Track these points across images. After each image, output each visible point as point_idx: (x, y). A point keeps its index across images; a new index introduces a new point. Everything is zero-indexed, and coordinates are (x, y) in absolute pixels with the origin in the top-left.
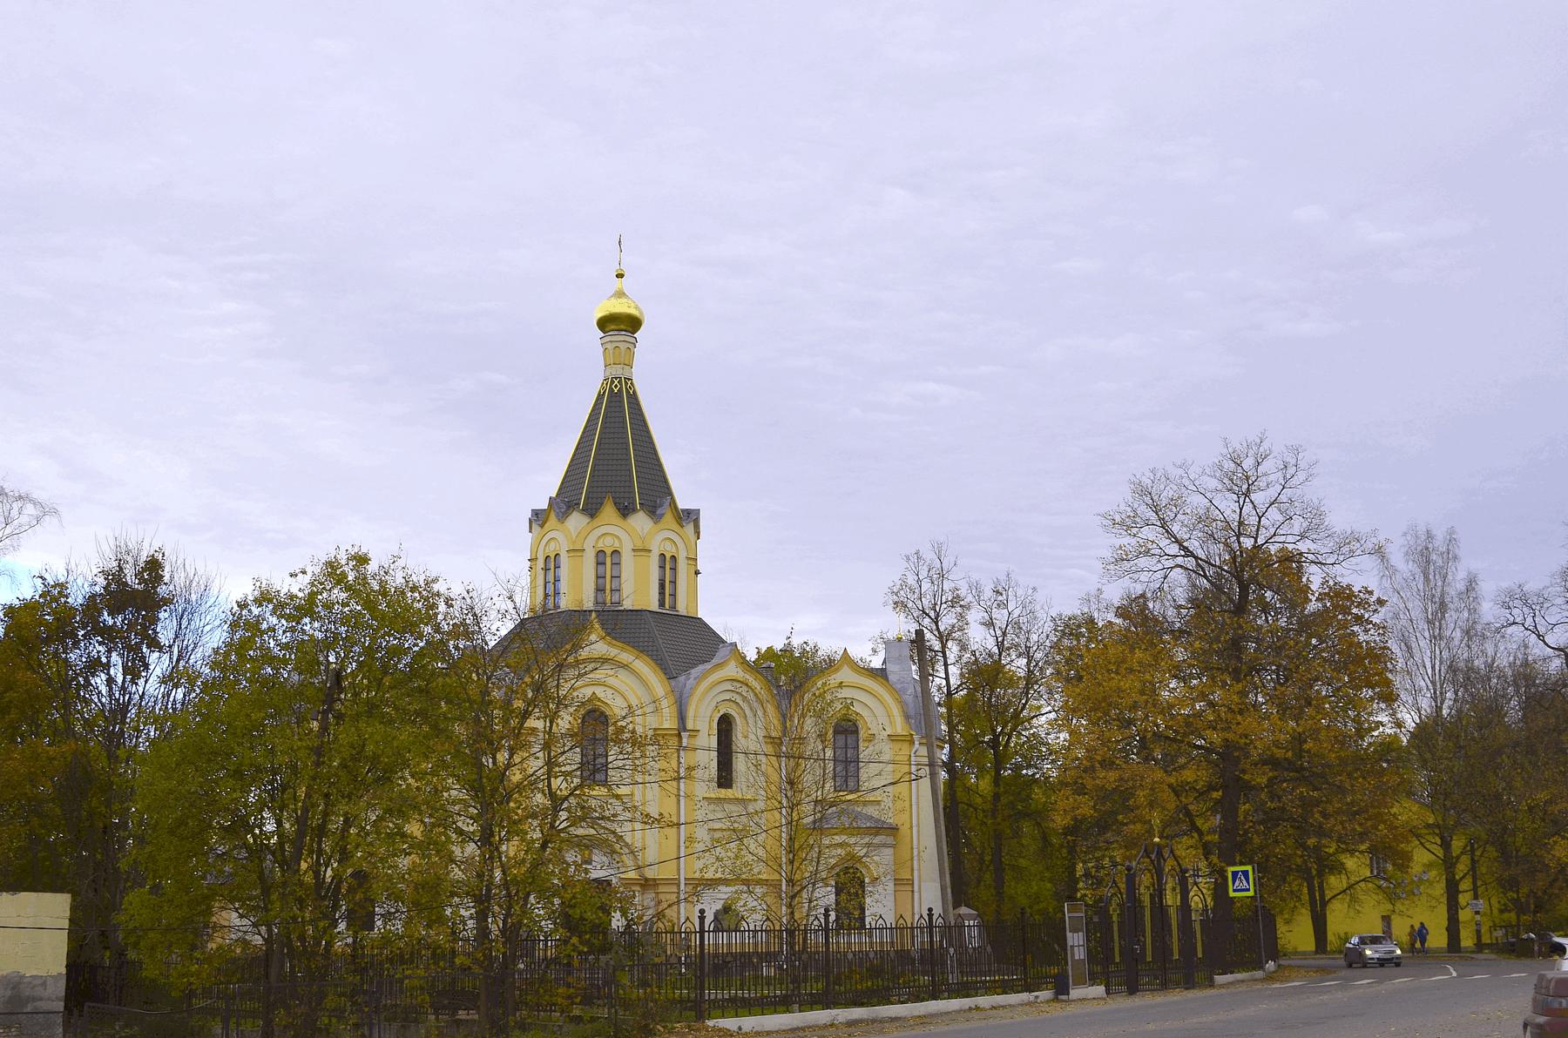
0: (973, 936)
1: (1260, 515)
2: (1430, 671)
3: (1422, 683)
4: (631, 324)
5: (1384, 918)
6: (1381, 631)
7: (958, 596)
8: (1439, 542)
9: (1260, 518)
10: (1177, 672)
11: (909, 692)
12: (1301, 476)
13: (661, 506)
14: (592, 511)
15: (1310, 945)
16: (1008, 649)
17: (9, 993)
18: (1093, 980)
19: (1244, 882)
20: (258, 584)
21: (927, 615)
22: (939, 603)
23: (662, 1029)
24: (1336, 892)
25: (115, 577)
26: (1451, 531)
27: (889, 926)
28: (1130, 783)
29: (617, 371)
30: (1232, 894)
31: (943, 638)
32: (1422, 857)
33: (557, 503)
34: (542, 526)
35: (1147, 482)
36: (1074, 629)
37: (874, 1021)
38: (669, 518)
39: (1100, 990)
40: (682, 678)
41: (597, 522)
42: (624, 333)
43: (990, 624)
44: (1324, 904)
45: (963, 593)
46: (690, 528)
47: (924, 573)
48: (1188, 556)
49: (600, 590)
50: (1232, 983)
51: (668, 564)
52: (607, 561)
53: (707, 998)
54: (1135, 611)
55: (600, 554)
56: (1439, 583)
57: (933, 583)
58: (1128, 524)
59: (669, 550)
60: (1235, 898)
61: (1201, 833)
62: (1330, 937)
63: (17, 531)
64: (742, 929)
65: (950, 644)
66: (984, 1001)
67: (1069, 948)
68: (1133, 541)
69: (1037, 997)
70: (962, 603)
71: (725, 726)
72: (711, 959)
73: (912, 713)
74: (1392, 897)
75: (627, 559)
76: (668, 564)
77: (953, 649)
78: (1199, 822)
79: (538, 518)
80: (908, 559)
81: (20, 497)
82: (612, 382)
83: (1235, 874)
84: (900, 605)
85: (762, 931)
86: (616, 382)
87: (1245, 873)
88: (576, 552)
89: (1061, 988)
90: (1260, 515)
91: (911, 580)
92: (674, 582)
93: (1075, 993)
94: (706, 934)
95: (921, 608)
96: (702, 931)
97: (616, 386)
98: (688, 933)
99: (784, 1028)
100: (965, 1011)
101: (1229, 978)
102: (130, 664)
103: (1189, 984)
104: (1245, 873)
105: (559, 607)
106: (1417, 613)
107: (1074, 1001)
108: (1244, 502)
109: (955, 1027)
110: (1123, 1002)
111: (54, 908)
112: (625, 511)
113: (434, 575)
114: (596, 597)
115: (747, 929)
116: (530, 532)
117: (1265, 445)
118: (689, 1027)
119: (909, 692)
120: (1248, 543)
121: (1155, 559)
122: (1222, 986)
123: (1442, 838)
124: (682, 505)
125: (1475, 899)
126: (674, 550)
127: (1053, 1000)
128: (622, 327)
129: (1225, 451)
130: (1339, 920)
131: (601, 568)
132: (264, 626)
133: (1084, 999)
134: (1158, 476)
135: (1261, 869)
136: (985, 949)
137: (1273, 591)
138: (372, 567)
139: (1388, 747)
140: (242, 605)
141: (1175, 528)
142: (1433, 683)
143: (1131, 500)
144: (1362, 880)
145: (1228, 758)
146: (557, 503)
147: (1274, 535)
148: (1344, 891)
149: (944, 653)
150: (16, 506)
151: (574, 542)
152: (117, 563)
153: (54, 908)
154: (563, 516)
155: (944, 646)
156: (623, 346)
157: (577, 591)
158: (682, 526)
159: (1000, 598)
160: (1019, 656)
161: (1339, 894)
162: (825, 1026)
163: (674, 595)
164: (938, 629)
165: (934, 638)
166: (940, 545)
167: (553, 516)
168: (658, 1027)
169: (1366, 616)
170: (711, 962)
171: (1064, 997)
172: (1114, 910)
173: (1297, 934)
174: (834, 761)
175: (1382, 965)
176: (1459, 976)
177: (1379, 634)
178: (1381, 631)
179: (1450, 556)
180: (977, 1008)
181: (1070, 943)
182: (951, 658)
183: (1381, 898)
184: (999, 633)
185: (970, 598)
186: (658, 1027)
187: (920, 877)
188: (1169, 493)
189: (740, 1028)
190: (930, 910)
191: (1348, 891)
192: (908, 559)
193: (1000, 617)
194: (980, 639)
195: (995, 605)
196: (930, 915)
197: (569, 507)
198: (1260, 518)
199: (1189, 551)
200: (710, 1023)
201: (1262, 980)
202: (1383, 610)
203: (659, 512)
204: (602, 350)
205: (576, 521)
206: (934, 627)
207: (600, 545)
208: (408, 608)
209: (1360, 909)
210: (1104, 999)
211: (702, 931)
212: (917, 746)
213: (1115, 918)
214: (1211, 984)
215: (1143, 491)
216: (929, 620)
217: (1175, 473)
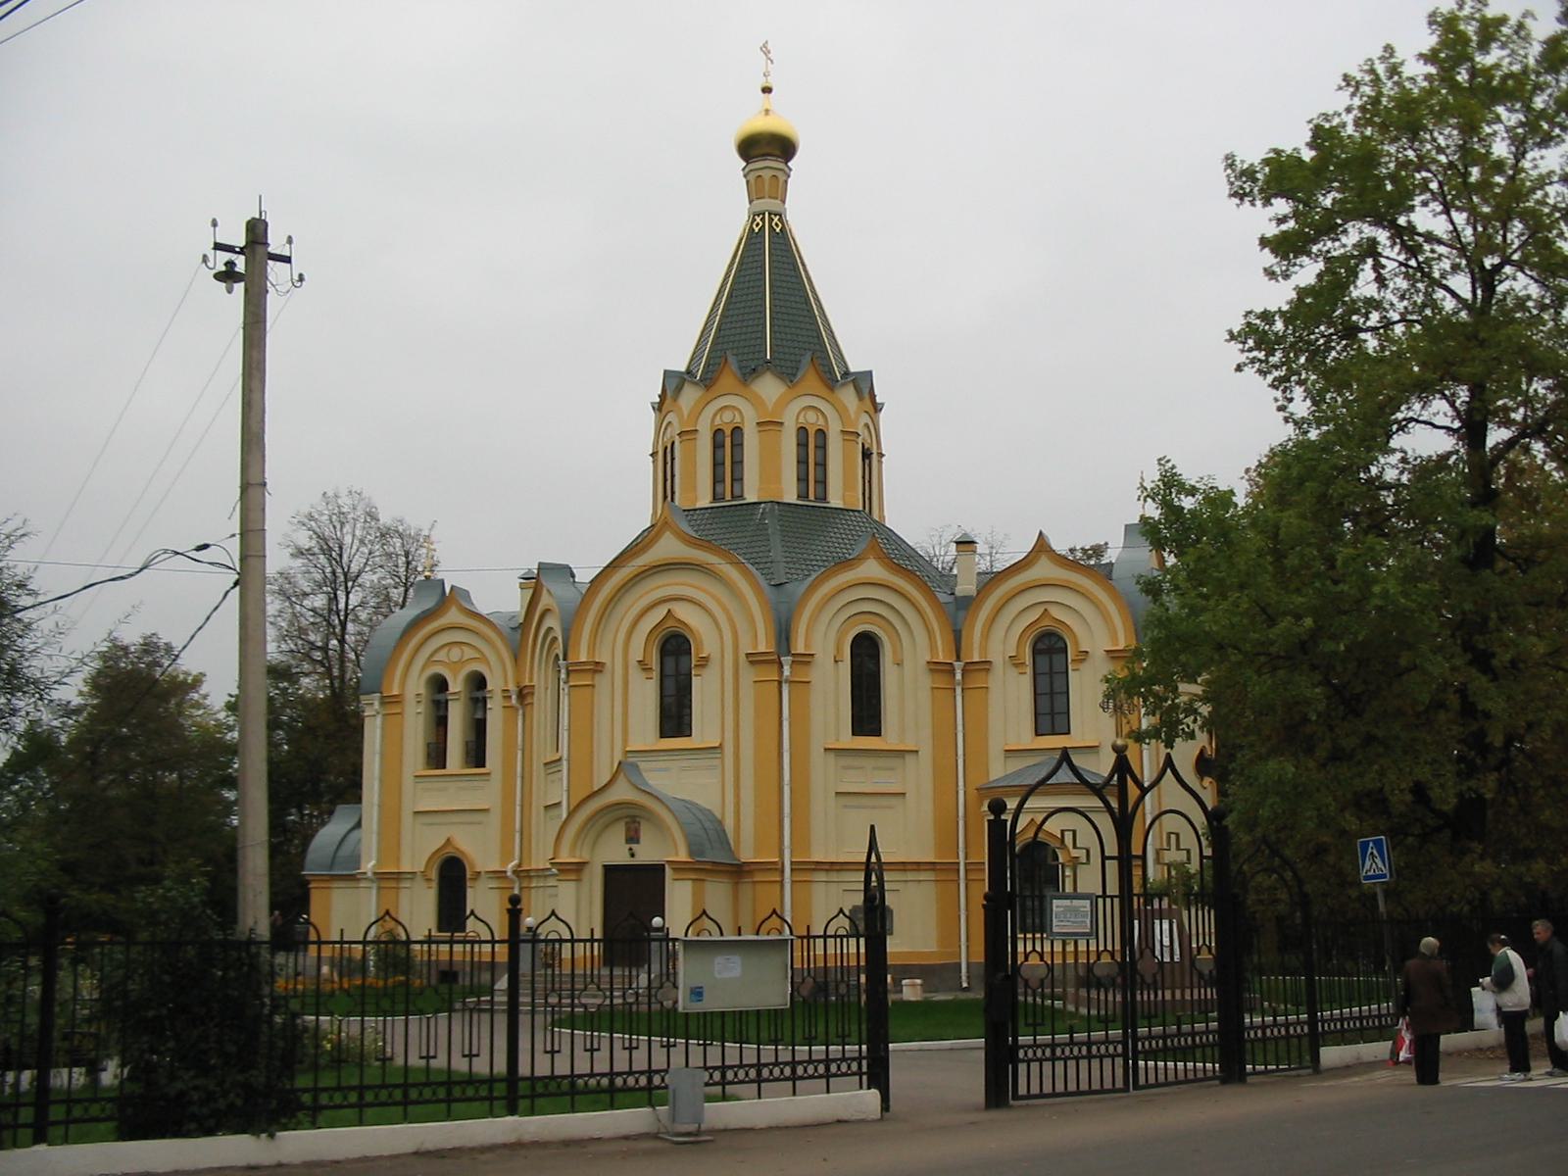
41: (718, 388)
51: (812, 447)
59: (812, 420)
71: (865, 652)
76: (812, 447)
97: (758, 225)
98: (842, 937)
102: (1292, 355)
112: (750, 373)
116: (659, 407)
126: (821, 421)
174: (572, 1075)
207: (718, 421)
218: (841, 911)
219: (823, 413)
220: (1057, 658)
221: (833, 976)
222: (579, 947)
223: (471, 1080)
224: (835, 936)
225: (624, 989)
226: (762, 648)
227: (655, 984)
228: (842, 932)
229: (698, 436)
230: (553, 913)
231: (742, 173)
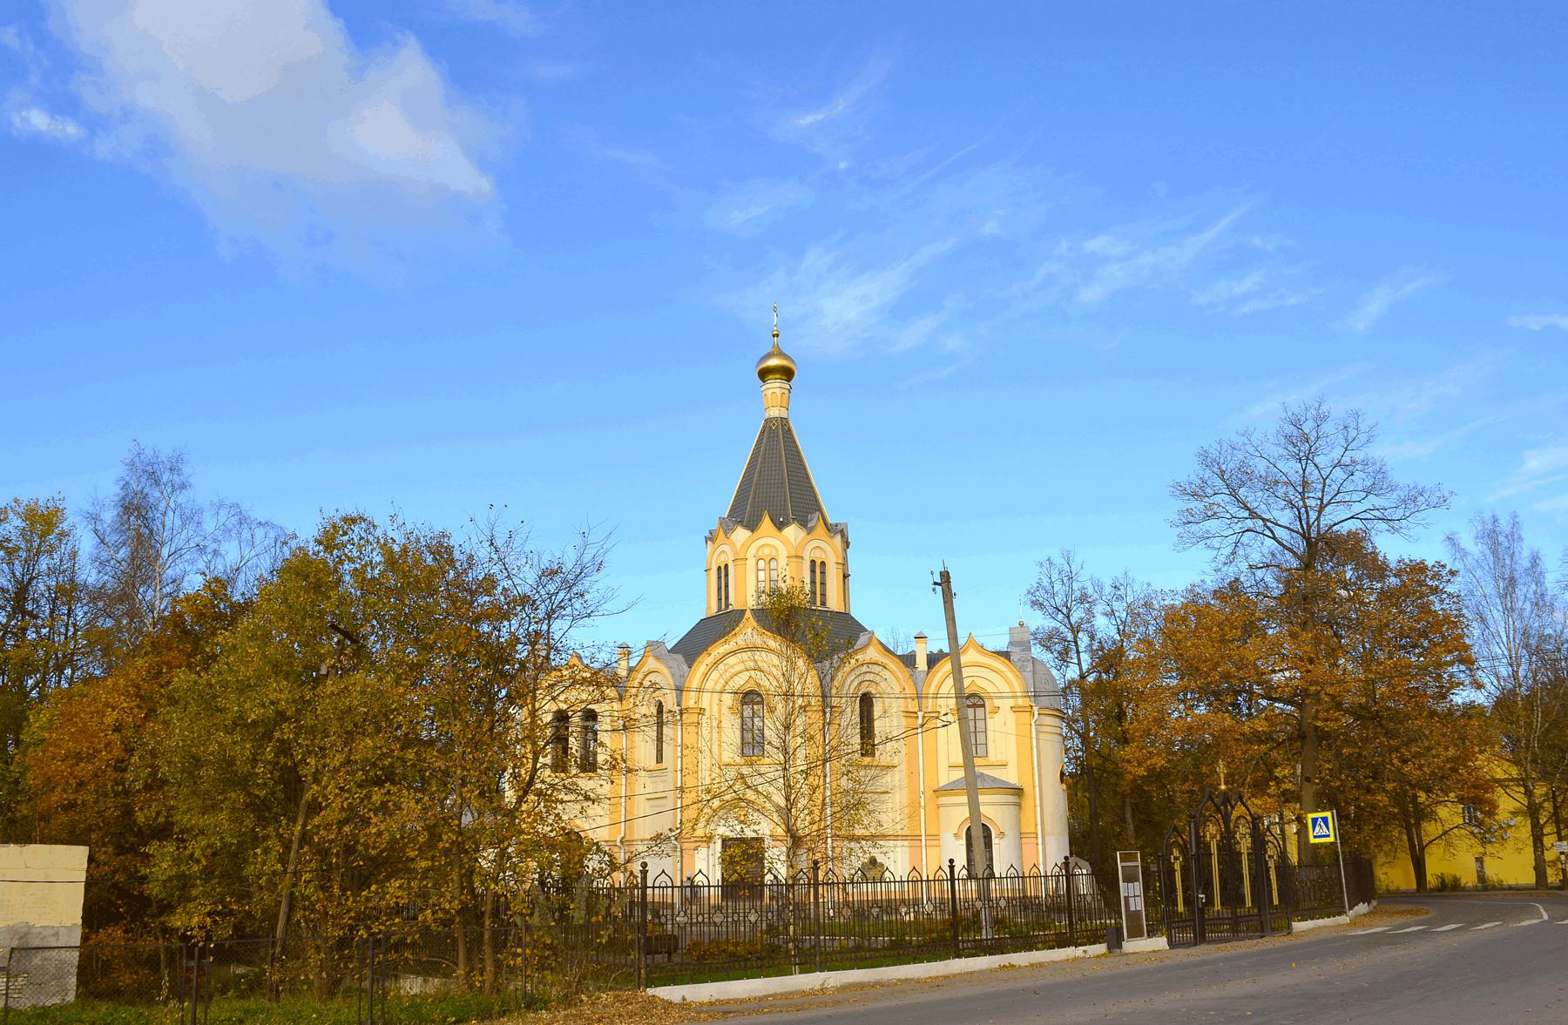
2: (1505, 639)
3: (1500, 652)
5: (1477, 859)
6: (1455, 600)
8: (1504, 525)
9: (1324, 480)
12: (1363, 438)
14: (752, 526)
19: (1324, 828)
22: (1070, 601)
24: (1432, 838)
26: (1514, 516)
27: (925, 878)
30: (1313, 841)
31: (1075, 630)
32: (1507, 803)
35: (1213, 453)
38: (821, 529)
44: (1422, 849)
45: (1090, 591)
47: (1055, 576)
56: (1508, 562)
59: (819, 557)
62: (1429, 877)
64: (888, 880)
65: (1080, 635)
68: (1201, 506)
69: (1085, 952)
72: (962, 904)
74: (1484, 842)
77: (1084, 640)
83: (1315, 821)
84: (1036, 604)
91: (1045, 583)
94: (956, 881)
96: (952, 880)
98: (663, 887)
104: (1325, 820)
106: (1490, 589)
108: (1307, 464)
115: (892, 880)
117: (1324, 408)
123: (1526, 787)
125: (1559, 841)
129: (1283, 416)
130: (1436, 866)
135: (1341, 817)
136: (935, 907)
137: (1543, 852)
139: (1470, 710)
142: (1509, 650)
144: (1456, 827)
148: (1440, 837)
149: (1076, 642)
155: (1075, 637)
161: (1435, 840)
166: (1069, 552)
169: (1441, 587)
173: (1394, 874)
176: (1552, 918)
177: (1453, 602)
178: (1455, 600)
179: (1514, 536)
182: (1082, 646)
183: (1473, 842)
187: (1043, 830)
189: (684, 999)
190: (951, 861)
191: (1443, 837)
192: (1041, 565)
193: (1120, 607)
194: (1105, 628)
196: (952, 868)
198: (1324, 480)
202: (1459, 579)
207: (760, 554)
209: (1455, 853)
211: (952, 880)
216: (1062, 615)
218: (1056, 864)
219: (824, 550)
220: (980, 711)
221: (994, 895)
222: (657, 890)
224: (659, 887)
225: (733, 914)
227: (974, 900)
228: (965, 877)
230: (663, 871)
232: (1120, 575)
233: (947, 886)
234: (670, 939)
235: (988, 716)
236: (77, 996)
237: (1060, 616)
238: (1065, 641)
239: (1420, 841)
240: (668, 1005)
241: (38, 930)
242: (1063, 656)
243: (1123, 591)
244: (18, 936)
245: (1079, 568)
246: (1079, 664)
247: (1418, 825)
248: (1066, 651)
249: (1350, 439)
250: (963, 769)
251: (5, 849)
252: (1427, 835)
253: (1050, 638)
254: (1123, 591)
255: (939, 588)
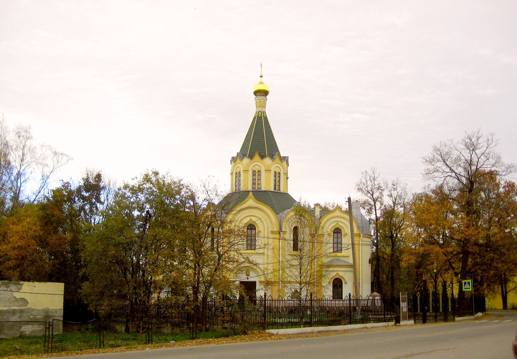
0: (379, 303)
1: (479, 158)
4: (265, 93)
7: (380, 186)
10: (454, 213)
11: (359, 219)
12: (494, 144)
13: (275, 155)
14: (251, 157)
15: (501, 306)
16: (397, 204)
17: (45, 314)
18: (410, 318)
20: (124, 182)
21: (369, 193)
22: (373, 189)
23: (250, 332)
25: (87, 180)
27: (363, 299)
28: (428, 252)
29: (260, 109)
31: (375, 201)
33: (240, 155)
34: (235, 162)
35: (438, 146)
36: (419, 198)
37: (328, 331)
38: (277, 160)
39: (412, 322)
40: (281, 214)
41: (253, 160)
42: (262, 96)
43: (391, 196)
44: (506, 293)
45: (382, 185)
46: (285, 163)
47: (368, 178)
48: (452, 172)
49: (254, 184)
50: (461, 320)
51: (277, 175)
52: (256, 174)
53: (266, 322)
54: (439, 191)
55: (254, 172)
57: (371, 181)
58: (431, 161)
59: (278, 170)
60: (466, 291)
61: (454, 269)
63: (61, 165)
65: (377, 203)
66: (369, 325)
67: (401, 307)
68: (433, 167)
69: (388, 324)
70: (381, 189)
73: (360, 226)
75: (263, 173)
76: (277, 175)
77: (378, 205)
78: (453, 265)
79: (234, 160)
80: (363, 173)
81: (62, 154)
82: (259, 113)
83: (465, 283)
84: (360, 189)
85: (287, 300)
86: (260, 113)
87: (469, 283)
88: (246, 171)
89: (398, 321)
90: (479, 158)
91: (364, 181)
92: (279, 181)
93: (402, 323)
95: (367, 190)
96: (350, 300)
97: (260, 114)
99: (294, 333)
100: (361, 328)
101: (461, 318)
103: (446, 320)
105: (240, 190)
107: (402, 325)
109: (355, 334)
110: (421, 326)
111: (59, 288)
112: (262, 157)
113: (181, 179)
114: (253, 186)
116: (231, 164)
118: (259, 332)
119: (359, 219)
120: (474, 168)
121: (440, 173)
122: (458, 321)
124: (282, 154)
127: (394, 325)
128: (262, 94)
131: (254, 176)
132: (126, 196)
133: (406, 325)
134: (442, 144)
135: (475, 281)
138: (160, 176)
140: (119, 189)
141: (448, 163)
143: (433, 152)
145: (464, 243)
146: (240, 155)
147: (483, 165)
148: (514, 288)
150: (60, 157)
151: (245, 168)
152: (87, 176)
153: (59, 288)
154: (242, 159)
155: (375, 203)
156: (262, 101)
157: (247, 184)
158: (282, 162)
159: (394, 187)
160: (401, 207)
161: (512, 290)
162: (310, 333)
163: (279, 186)
164: (373, 197)
165: (372, 201)
167: (238, 159)
168: (249, 332)
170: (268, 311)
171: (398, 324)
172: (418, 295)
175: (319, 335)
180: (366, 328)
181: (401, 306)
182: (377, 208)
184: (394, 199)
185: (384, 187)
186: (249, 332)
187: (362, 282)
188: (446, 150)
189: (278, 333)
190: (350, 294)
192: (363, 173)
193: (394, 194)
194: (388, 201)
195: (393, 189)
196: (350, 296)
197: (243, 156)
199: (453, 170)
200: (267, 331)
201: (472, 319)
203: (274, 157)
204: (255, 102)
205: (246, 160)
206: (372, 197)
207: (254, 169)
208: (172, 190)
210: (413, 325)
211: (350, 300)
212: (361, 238)
213: (418, 298)
214: (454, 320)
215: (436, 149)
216: (370, 194)
217: (448, 143)
220: (339, 235)
223: (280, 323)
224: (269, 300)
226: (275, 230)
228: (270, 299)
229: (249, 172)
231: (254, 99)
232: (395, 179)
233: (348, 302)
234: (467, 299)
235: (342, 237)
236: (63, 331)
237: (369, 195)
238: (371, 205)
239: (506, 290)
240: (273, 334)
241: (51, 310)
242: (369, 212)
243: (396, 186)
244: (45, 312)
245: (378, 175)
246: (376, 214)
247: (506, 284)
248: (371, 209)
249: (489, 144)
250: (252, 230)
251: (40, 284)
252: (509, 287)
253: (364, 203)
254: (396, 186)
255: (347, 203)
